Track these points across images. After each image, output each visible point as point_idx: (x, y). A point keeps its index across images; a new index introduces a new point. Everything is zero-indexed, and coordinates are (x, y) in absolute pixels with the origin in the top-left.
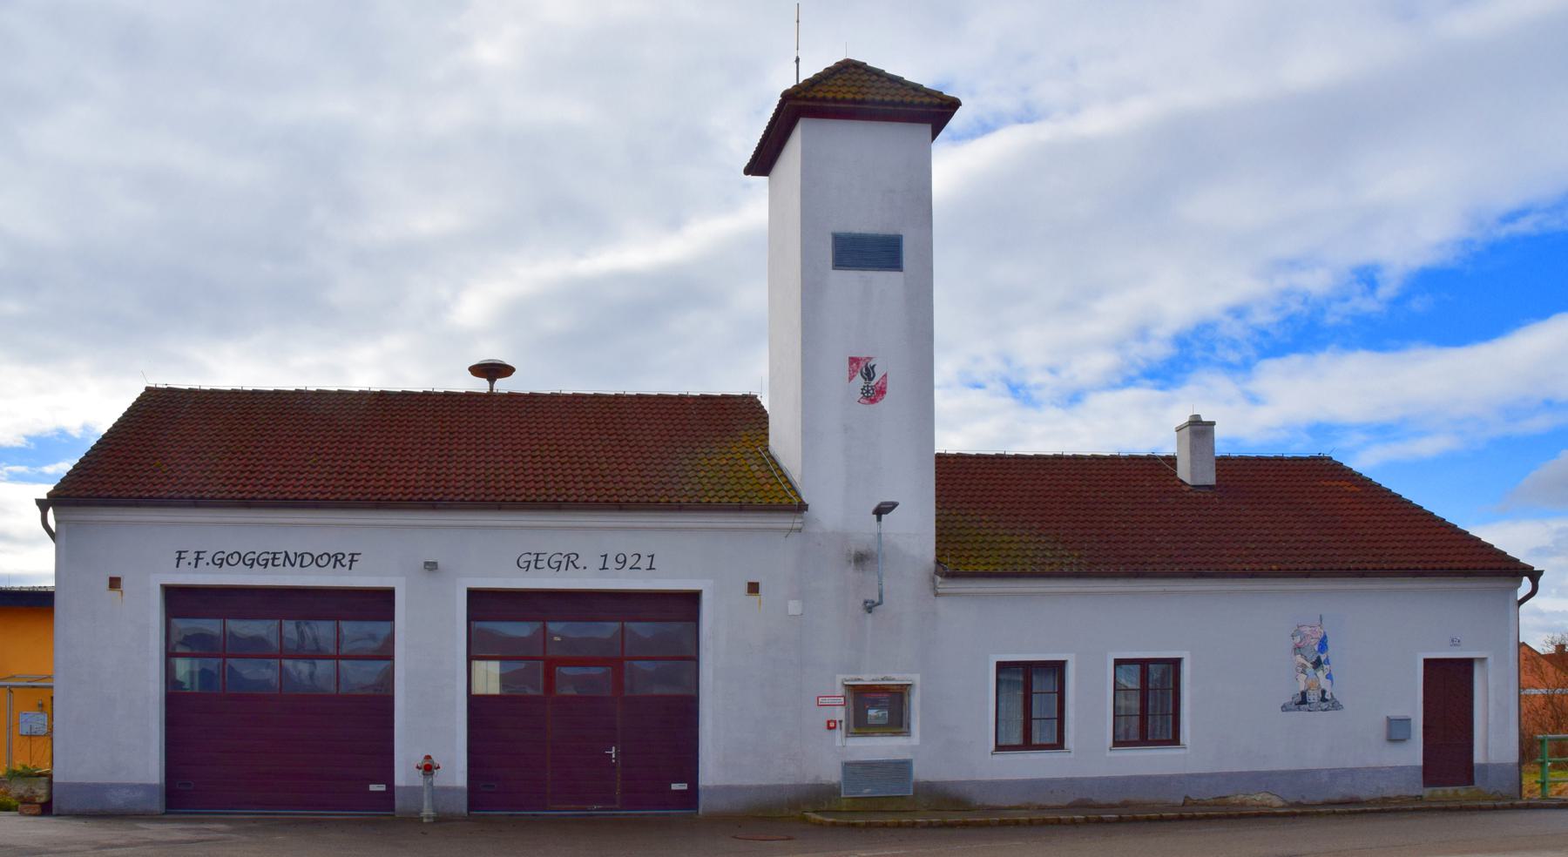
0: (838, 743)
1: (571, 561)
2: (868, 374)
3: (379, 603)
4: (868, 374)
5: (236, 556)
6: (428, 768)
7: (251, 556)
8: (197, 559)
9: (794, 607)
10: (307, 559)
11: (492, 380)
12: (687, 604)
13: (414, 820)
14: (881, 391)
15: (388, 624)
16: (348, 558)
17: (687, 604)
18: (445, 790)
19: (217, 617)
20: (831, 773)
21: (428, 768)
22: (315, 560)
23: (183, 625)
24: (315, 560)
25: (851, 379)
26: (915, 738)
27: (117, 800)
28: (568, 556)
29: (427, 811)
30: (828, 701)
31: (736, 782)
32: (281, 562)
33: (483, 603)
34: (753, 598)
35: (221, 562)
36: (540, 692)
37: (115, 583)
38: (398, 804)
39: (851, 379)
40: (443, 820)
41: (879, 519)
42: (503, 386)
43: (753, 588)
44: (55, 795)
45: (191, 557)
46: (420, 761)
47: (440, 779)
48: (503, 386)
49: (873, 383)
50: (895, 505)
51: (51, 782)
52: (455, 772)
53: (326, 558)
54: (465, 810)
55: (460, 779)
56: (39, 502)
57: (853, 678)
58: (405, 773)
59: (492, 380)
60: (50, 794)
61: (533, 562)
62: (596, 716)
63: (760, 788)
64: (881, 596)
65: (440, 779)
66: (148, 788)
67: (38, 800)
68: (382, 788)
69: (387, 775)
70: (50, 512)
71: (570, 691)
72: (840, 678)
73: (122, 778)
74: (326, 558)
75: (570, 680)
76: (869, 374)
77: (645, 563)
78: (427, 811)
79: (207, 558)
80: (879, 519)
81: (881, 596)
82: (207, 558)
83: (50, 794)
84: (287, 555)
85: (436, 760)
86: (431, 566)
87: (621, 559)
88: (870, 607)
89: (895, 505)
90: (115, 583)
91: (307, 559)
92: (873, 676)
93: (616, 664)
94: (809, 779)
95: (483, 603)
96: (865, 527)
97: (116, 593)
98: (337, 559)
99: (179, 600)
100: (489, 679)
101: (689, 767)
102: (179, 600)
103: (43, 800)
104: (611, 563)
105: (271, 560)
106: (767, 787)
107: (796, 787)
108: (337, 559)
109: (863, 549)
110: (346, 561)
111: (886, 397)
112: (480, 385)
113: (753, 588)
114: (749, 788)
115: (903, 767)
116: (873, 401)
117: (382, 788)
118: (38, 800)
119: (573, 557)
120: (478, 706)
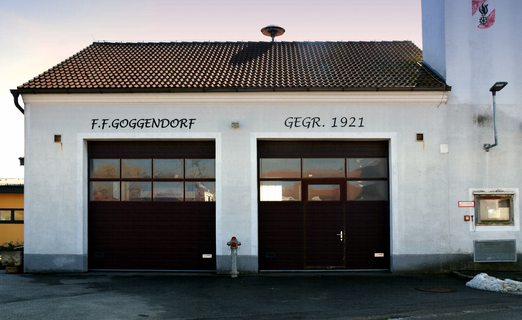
0: (471, 230)
1: (315, 122)
2: (484, 10)
3: (206, 149)
4: (484, 10)
5: (125, 122)
6: (234, 244)
7: (134, 122)
8: (104, 124)
9: (444, 149)
10: (166, 123)
11: (273, 36)
12: (381, 148)
13: (226, 276)
14: (492, 20)
15: (213, 160)
16: (189, 122)
17: (381, 148)
18: (246, 257)
19: (117, 158)
20: (468, 249)
21: (234, 244)
22: (170, 123)
23: (103, 165)
24: (170, 123)
25: (473, 14)
26: (517, 227)
27: (59, 265)
28: (314, 119)
29: (235, 272)
30: (465, 204)
31: (412, 253)
32: (150, 124)
33: (267, 148)
34: (420, 143)
35: (117, 125)
36: (300, 199)
37: (57, 138)
38: (218, 265)
39: (473, 14)
40: (244, 276)
41: (494, 94)
42: (278, 39)
43: (420, 137)
44: (25, 262)
45: (100, 123)
46: (229, 239)
47: (241, 251)
48: (278, 39)
49: (487, 15)
50: (505, 84)
51: (22, 254)
52: (251, 247)
53: (176, 122)
54: (256, 269)
55: (254, 251)
56: (12, 91)
57: (478, 190)
58: (221, 248)
59: (273, 36)
60: (22, 261)
61: (293, 123)
62: (333, 224)
63: (426, 256)
64: (496, 140)
65: (241, 251)
66: (76, 257)
67: (16, 264)
68: (210, 256)
69: (212, 249)
70: (20, 98)
71: (317, 198)
72: (471, 190)
73: (62, 251)
74: (176, 122)
75: (317, 193)
76: (484, 10)
77: (357, 123)
78: (235, 272)
79: (109, 123)
80: (494, 94)
81: (496, 140)
82: (109, 123)
83: (22, 261)
84: (154, 121)
85: (239, 239)
86: (236, 125)
87: (344, 120)
88: (487, 148)
89: (505, 84)
90: (57, 138)
91: (166, 123)
92: (491, 190)
93: (342, 182)
94: (454, 251)
95: (267, 148)
96: (485, 101)
97: (58, 144)
98: (182, 123)
99: (96, 149)
100: (273, 193)
101: (385, 243)
102: (96, 149)
103: (18, 264)
104: (338, 123)
105: (145, 124)
106: (430, 255)
107: (447, 256)
108: (182, 123)
109: (483, 114)
110: (187, 124)
111: (495, 23)
112: (268, 39)
113: (420, 137)
114: (420, 256)
115: (509, 245)
116: (487, 26)
117: (210, 256)
118: (16, 264)
119: (317, 120)
120: (265, 209)
